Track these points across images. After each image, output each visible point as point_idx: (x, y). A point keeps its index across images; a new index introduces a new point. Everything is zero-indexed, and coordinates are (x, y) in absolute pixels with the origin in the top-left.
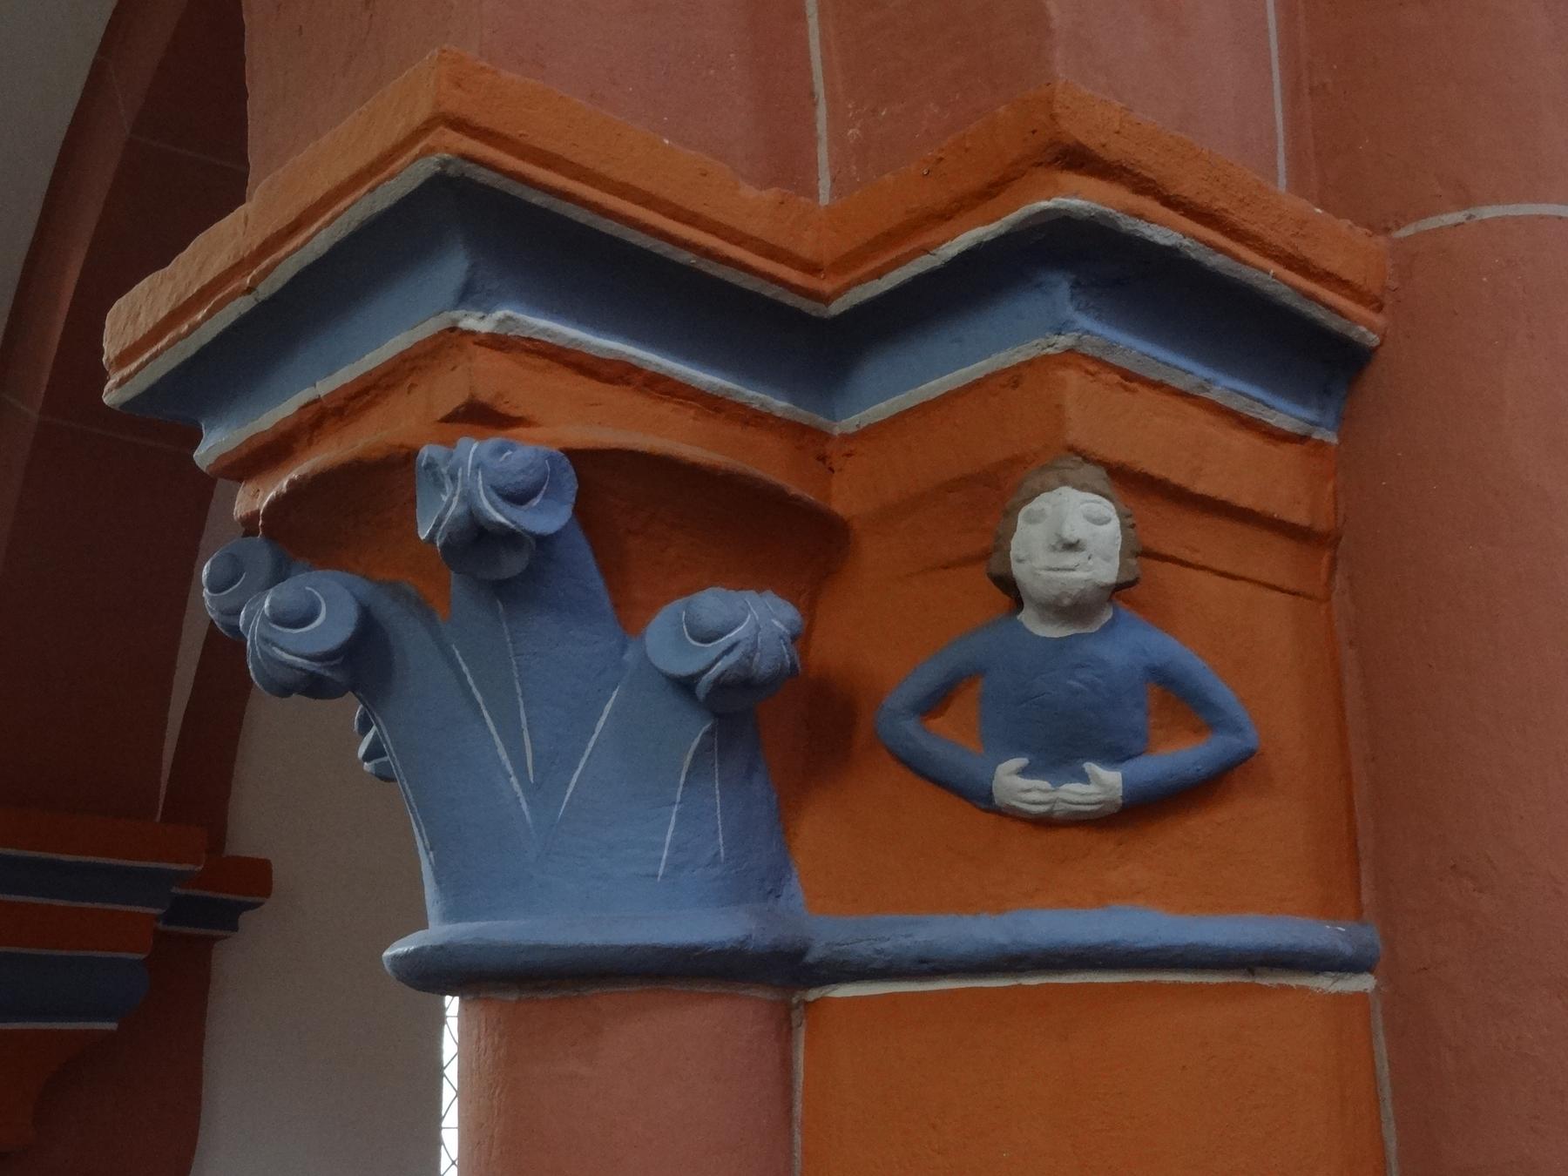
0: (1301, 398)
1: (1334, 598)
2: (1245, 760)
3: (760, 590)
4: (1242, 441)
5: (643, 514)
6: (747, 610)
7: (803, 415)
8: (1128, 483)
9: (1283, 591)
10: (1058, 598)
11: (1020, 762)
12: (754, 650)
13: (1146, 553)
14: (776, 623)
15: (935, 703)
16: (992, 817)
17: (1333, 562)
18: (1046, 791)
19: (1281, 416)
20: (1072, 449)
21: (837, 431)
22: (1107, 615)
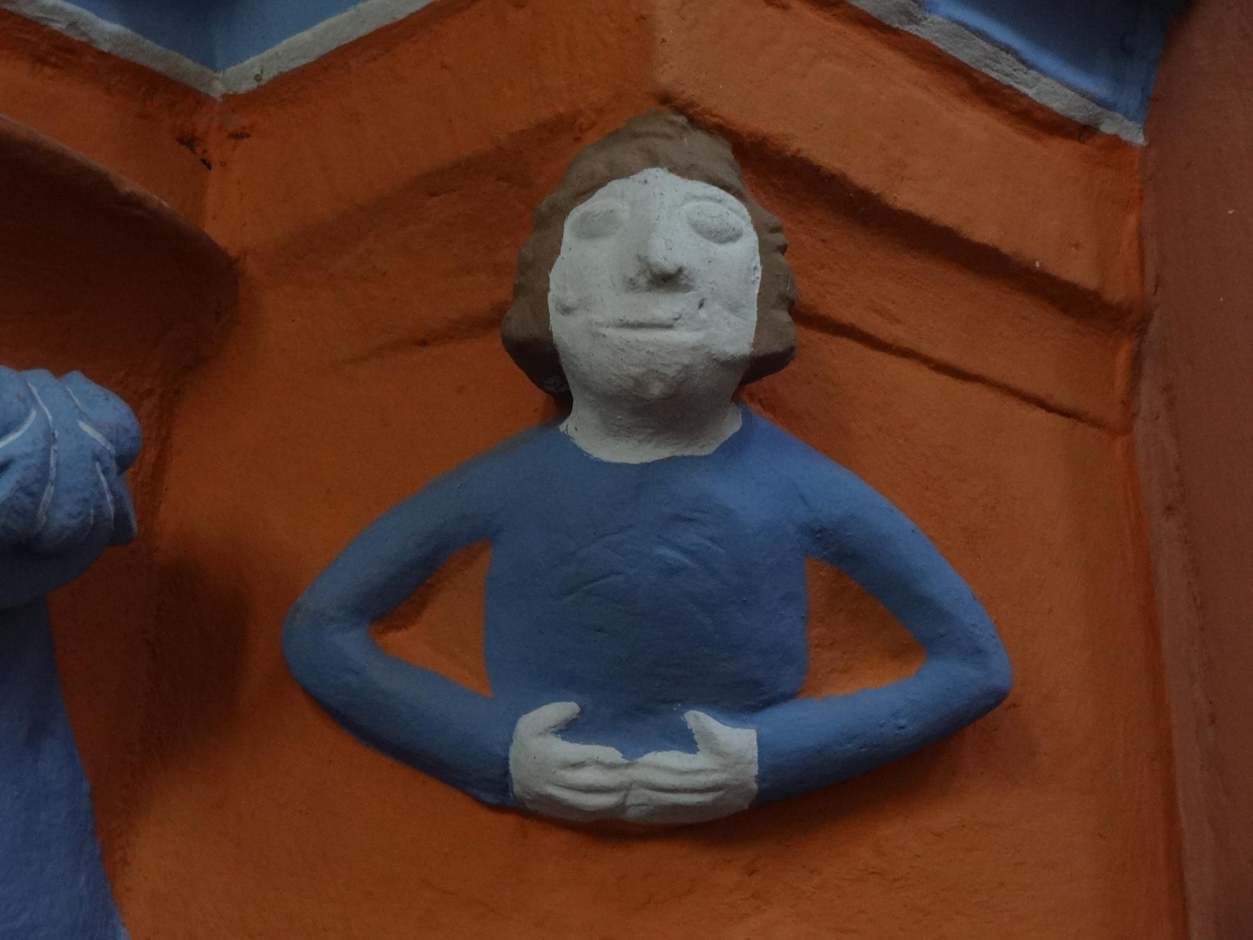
0: (1080, 57)
1: (1140, 428)
2: (989, 708)
3: (59, 371)
4: (978, 125)
6: (29, 400)
7: (150, 52)
8: (767, 171)
9: (1050, 409)
10: (638, 382)
11: (561, 710)
12: (43, 479)
13: (804, 316)
14: (87, 429)
15: (396, 601)
16: (509, 820)
17: (1136, 361)
18: (612, 767)
19: (1045, 84)
20: (665, 99)
21: (218, 89)
22: (732, 425)
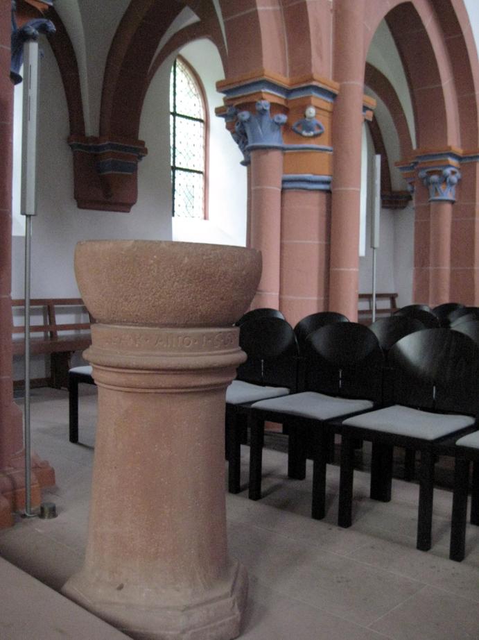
5: (275, 107)
8: (316, 107)
